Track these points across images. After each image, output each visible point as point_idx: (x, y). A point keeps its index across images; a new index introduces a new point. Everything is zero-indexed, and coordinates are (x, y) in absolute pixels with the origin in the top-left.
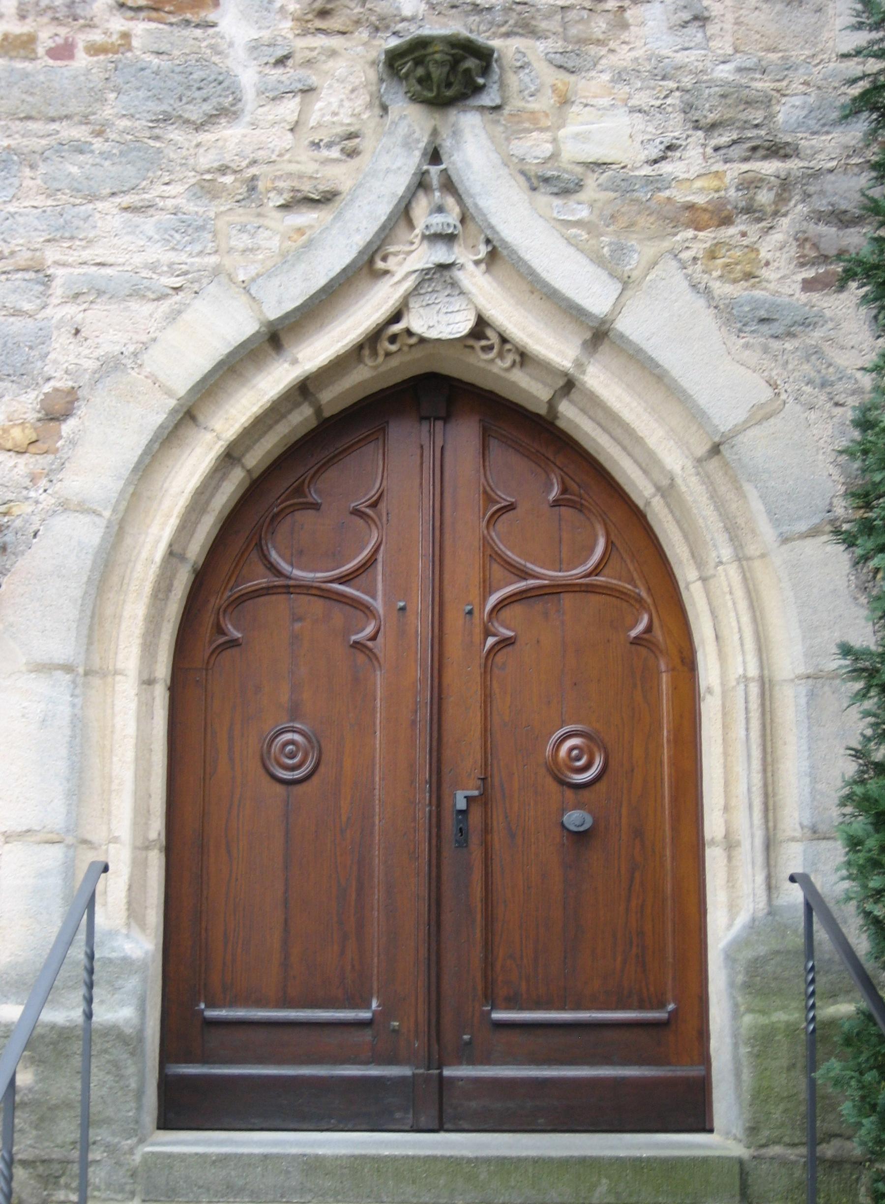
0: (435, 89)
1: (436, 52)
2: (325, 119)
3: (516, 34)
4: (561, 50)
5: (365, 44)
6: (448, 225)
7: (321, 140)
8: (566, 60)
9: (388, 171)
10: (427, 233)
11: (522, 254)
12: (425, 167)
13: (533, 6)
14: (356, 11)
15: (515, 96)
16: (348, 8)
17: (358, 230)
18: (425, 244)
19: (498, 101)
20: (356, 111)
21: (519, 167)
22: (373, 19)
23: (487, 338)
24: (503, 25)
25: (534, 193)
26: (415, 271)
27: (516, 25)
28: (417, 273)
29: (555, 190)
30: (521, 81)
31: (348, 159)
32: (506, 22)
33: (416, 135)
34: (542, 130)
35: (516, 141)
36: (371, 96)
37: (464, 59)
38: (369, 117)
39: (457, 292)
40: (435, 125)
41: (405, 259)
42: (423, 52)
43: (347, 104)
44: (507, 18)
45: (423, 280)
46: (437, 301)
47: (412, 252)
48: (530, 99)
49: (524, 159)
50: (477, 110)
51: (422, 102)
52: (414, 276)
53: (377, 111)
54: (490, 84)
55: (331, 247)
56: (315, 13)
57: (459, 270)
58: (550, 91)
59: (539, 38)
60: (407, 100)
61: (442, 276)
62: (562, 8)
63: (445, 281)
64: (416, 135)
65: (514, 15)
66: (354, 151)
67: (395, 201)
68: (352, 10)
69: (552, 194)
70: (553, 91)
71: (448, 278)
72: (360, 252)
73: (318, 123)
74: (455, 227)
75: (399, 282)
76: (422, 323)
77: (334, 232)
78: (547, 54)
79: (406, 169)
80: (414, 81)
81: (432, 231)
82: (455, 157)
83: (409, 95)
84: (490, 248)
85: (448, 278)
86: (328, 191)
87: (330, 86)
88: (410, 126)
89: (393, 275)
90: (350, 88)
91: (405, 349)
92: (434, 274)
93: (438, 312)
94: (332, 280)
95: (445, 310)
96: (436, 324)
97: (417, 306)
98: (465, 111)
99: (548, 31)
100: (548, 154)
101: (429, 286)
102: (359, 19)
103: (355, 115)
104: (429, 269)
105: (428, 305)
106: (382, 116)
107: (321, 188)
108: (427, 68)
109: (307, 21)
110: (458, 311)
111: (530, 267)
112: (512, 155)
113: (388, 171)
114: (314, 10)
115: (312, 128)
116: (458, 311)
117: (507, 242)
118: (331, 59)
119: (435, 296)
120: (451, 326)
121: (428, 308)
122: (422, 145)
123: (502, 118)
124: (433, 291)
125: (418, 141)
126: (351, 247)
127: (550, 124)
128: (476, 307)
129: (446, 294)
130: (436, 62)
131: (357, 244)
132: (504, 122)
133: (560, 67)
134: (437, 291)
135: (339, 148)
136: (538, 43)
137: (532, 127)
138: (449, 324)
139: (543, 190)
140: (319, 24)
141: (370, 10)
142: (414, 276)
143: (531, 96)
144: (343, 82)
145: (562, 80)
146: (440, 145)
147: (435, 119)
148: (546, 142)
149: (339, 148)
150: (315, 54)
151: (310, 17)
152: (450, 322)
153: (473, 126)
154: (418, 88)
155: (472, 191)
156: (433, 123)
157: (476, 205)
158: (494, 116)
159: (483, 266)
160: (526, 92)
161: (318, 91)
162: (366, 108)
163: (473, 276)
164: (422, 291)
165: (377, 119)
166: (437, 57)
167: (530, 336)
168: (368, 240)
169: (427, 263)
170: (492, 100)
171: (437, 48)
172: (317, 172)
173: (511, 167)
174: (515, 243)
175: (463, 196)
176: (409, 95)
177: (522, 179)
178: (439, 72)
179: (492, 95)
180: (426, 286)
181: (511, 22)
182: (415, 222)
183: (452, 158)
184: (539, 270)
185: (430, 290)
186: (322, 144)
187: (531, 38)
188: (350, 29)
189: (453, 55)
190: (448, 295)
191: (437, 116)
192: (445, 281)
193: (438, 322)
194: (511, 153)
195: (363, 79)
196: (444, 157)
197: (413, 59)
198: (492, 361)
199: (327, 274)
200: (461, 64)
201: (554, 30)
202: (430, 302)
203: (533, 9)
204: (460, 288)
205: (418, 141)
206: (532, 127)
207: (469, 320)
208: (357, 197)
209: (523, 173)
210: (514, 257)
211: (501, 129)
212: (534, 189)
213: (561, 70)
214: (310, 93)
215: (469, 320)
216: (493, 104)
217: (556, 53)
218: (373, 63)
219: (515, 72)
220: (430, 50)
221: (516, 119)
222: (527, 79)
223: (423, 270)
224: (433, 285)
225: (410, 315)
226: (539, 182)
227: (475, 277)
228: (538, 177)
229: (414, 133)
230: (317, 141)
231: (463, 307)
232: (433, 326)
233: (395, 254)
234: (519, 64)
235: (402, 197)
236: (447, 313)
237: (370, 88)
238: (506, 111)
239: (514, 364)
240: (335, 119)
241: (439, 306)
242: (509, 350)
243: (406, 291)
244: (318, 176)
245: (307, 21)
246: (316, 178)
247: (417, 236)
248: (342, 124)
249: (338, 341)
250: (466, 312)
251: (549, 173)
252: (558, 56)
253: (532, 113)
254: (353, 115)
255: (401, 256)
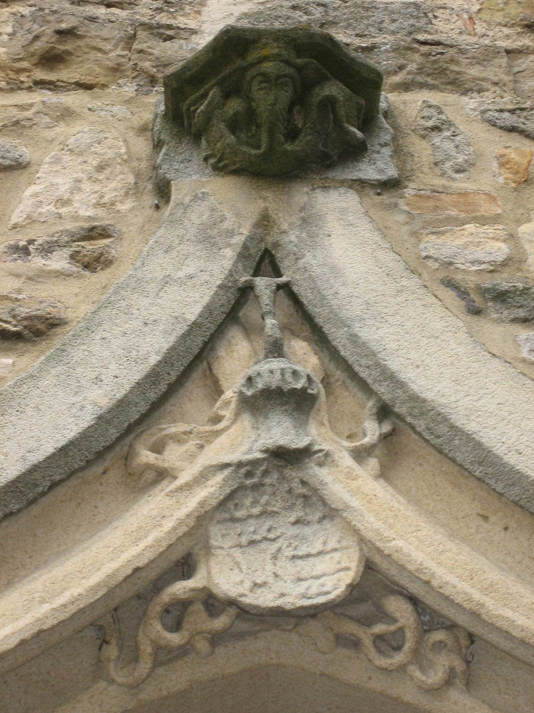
0: (264, 137)
1: (265, 59)
2: (44, 210)
3: (422, 86)
4: (511, 107)
5: (128, 102)
6: (295, 373)
7: (31, 242)
8: (522, 120)
9: (167, 281)
10: (249, 393)
11: (459, 420)
12: (244, 278)
13: (452, 46)
14: (112, 55)
15: (426, 169)
16: (99, 50)
17: (98, 380)
18: (246, 420)
19: (392, 172)
20: (106, 199)
21: (441, 275)
22: (147, 64)
23: (392, 620)
24: (395, 73)
25: (476, 318)
26: (226, 466)
27: (420, 70)
28: (227, 472)
29: (521, 313)
30: (435, 148)
31: (87, 273)
32: (401, 68)
33: (226, 225)
34: (483, 221)
35: (433, 237)
36: (138, 175)
37: (322, 79)
38: (131, 210)
39: (318, 515)
40: (266, 209)
41: (202, 447)
42: (239, 63)
43: (87, 186)
44: (402, 61)
45: (241, 488)
46: (271, 536)
47: (217, 434)
48: (457, 176)
49: (451, 263)
50: (351, 187)
51: (236, 172)
52: (219, 477)
53: (150, 200)
54: (373, 144)
55: (37, 408)
56: (34, 60)
57: (320, 465)
58: (495, 165)
59: (465, 93)
60: (209, 170)
61: (283, 478)
62: (508, 52)
63: (290, 491)
64: (226, 225)
65: (417, 57)
66: (97, 260)
67: (181, 329)
68: (105, 52)
69: (515, 320)
70: (502, 165)
71: (295, 484)
72: (100, 418)
73: (29, 217)
74: (309, 379)
75: (188, 487)
76: (239, 578)
77: (43, 383)
78: (484, 112)
79: (205, 277)
80: (222, 126)
81: (260, 386)
82: (308, 259)
83: (212, 161)
84: (386, 428)
85: (295, 484)
86: (37, 317)
87: (57, 160)
88: (213, 210)
89: (175, 478)
90: (95, 163)
91: (202, 645)
92: (265, 473)
93: (275, 557)
94: (35, 469)
95: (289, 552)
96: (271, 580)
97: (227, 544)
98: (325, 188)
99: (484, 79)
100: (500, 259)
101: (255, 503)
102: (119, 65)
103: (104, 205)
104: (254, 463)
105: (252, 543)
106: (157, 207)
107: (24, 311)
108: (249, 99)
109: (19, 71)
110: (320, 553)
111: (479, 445)
112: (427, 257)
113: (167, 281)
114: (33, 55)
115: (15, 227)
116: (320, 553)
117: (424, 401)
118: (62, 124)
119: (268, 523)
120: (304, 585)
121: (251, 550)
122: (238, 240)
123: (401, 203)
124: (263, 513)
125: (231, 233)
126: (82, 408)
127: (499, 211)
128: (362, 540)
129: (292, 519)
130: (265, 77)
131: (95, 404)
132: (406, 208)
133: (512, 130)
134: (273, 514)
135: (67, 252)
136: (465, 99)
137: (463, 215)
138: (300, 580)
139: (495, 316)
140: (40, 74)
141: (141, 51)
142: (219, 477)
143: (458, 171)
144: (81, 154)
145: (517, 148)
146: (276, 245)
147: (265, 199)
148: (496, 239)
149: (67, 252)
150: (29, 114)
151: (25, 64)
152: (304, 574)
153: (343, 211)
154: (231, 139)
155: (344, 314)
156: (261, 204)
157: (354, 339)
158: (386, 198)
159: (373, 463)
160: (448, 165)
161: (32, 169)
162: (127, 194)
163: (350, 476)
164: (240, 514)
165: (150, 212)
166: (268, 67)
167: (486, 590)
168: (119, 396)
169: (250, 450)
170: (381, 171)
171: (266, 52)
172: (19, 291)
173: (425, 275)
174: (443, 401)
175: (327, 328)
176: (212, 161)
177: (449, 295)
178: (271, 98)
179: (380, 164)
180: (248, 502)
181: (412, 67)
182: (224, 383)
183: (301, 263)
184: (499, 450)
185: (256, 511)
186: (31, 248)
187: (452, 92)
188: (102, 80)
189: (299, 69)
190: (297, 522)
191: (269, 194)
192: (290, 491)
193: (276, 575)
194: (424, 254)
195: (123, 150)
196: (284, 265)
197: (219, 84)
198: (402, 668)
199: (24, 458)
200: (317, 90)
201: (495, 79)
202: (258, 537)
203: (452, 52)
204: (324, 503)
205: (231, 233)
206: (463, 215)
207: (347, 569)
208: (100, 324)
209: (450, 284)
210: (443, 429)
211: (401, 218)
212: (477, 312)
213: (514, 135)
214: (16, 173)
215: (347, 569)
216: (383, 177)
217: (501, 111)
218: (143, 129)
219: (423, 137)
220: (252, 57)
221: (431, 203)
222: (448, 146)
223: (240, 465)
224: (264, 499)
225: (213, 562)
226: (486, 300)
227: (356, 479)
228: (483, 291)
229: (223, 219)
230: (22, 243)
231: (332, 544)
232: (264, 584)
233: (178, 439)
234: (430, 124)
235: (195, 326)
236: (294, 557)
237: (135, 164)
238: (409, 191)
239: (449, 682)
240: (63, 210)
241: (276, 545)
242: (440, 645)
243: (202, 504)
244: (20, 297)
245: (19, 71)
246: (17, 300)
247: (227, 403)
248: (75, 218)
249: (43, 601)
250: (337, 556)
251: (505, 286)
252: (506, 115)
253: (464, 194)
254: (98, 205)
255: (191, 445)
